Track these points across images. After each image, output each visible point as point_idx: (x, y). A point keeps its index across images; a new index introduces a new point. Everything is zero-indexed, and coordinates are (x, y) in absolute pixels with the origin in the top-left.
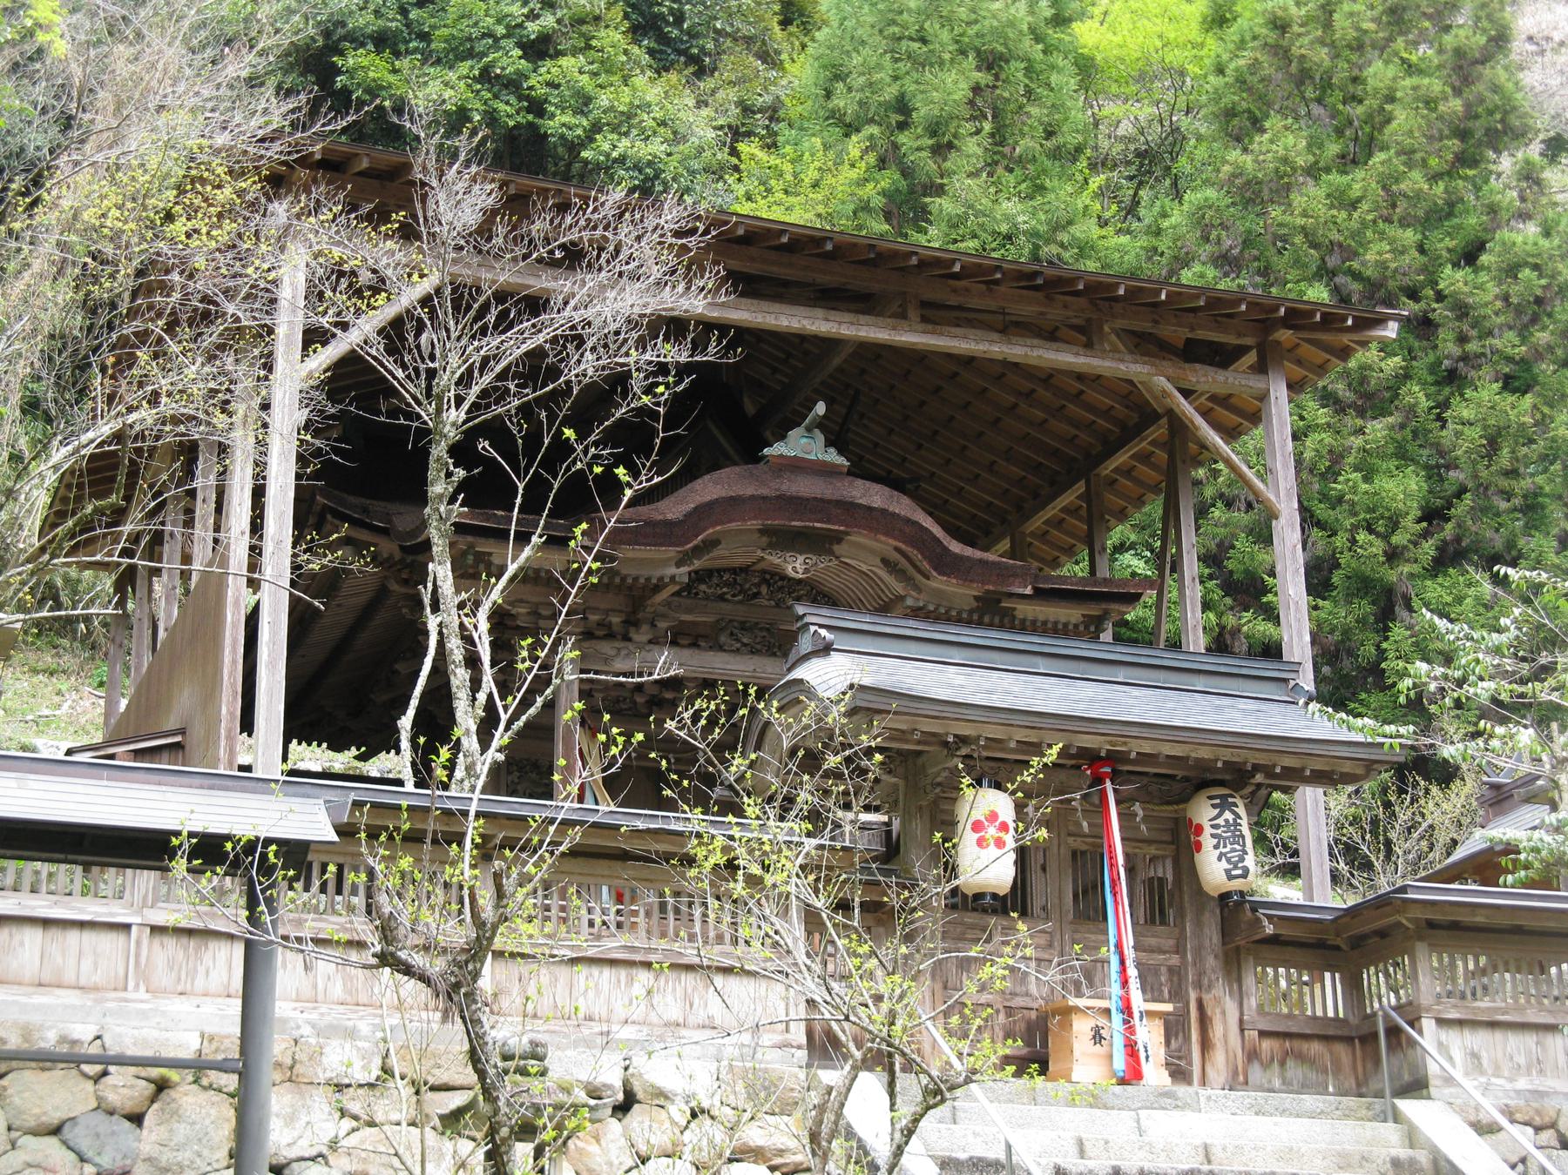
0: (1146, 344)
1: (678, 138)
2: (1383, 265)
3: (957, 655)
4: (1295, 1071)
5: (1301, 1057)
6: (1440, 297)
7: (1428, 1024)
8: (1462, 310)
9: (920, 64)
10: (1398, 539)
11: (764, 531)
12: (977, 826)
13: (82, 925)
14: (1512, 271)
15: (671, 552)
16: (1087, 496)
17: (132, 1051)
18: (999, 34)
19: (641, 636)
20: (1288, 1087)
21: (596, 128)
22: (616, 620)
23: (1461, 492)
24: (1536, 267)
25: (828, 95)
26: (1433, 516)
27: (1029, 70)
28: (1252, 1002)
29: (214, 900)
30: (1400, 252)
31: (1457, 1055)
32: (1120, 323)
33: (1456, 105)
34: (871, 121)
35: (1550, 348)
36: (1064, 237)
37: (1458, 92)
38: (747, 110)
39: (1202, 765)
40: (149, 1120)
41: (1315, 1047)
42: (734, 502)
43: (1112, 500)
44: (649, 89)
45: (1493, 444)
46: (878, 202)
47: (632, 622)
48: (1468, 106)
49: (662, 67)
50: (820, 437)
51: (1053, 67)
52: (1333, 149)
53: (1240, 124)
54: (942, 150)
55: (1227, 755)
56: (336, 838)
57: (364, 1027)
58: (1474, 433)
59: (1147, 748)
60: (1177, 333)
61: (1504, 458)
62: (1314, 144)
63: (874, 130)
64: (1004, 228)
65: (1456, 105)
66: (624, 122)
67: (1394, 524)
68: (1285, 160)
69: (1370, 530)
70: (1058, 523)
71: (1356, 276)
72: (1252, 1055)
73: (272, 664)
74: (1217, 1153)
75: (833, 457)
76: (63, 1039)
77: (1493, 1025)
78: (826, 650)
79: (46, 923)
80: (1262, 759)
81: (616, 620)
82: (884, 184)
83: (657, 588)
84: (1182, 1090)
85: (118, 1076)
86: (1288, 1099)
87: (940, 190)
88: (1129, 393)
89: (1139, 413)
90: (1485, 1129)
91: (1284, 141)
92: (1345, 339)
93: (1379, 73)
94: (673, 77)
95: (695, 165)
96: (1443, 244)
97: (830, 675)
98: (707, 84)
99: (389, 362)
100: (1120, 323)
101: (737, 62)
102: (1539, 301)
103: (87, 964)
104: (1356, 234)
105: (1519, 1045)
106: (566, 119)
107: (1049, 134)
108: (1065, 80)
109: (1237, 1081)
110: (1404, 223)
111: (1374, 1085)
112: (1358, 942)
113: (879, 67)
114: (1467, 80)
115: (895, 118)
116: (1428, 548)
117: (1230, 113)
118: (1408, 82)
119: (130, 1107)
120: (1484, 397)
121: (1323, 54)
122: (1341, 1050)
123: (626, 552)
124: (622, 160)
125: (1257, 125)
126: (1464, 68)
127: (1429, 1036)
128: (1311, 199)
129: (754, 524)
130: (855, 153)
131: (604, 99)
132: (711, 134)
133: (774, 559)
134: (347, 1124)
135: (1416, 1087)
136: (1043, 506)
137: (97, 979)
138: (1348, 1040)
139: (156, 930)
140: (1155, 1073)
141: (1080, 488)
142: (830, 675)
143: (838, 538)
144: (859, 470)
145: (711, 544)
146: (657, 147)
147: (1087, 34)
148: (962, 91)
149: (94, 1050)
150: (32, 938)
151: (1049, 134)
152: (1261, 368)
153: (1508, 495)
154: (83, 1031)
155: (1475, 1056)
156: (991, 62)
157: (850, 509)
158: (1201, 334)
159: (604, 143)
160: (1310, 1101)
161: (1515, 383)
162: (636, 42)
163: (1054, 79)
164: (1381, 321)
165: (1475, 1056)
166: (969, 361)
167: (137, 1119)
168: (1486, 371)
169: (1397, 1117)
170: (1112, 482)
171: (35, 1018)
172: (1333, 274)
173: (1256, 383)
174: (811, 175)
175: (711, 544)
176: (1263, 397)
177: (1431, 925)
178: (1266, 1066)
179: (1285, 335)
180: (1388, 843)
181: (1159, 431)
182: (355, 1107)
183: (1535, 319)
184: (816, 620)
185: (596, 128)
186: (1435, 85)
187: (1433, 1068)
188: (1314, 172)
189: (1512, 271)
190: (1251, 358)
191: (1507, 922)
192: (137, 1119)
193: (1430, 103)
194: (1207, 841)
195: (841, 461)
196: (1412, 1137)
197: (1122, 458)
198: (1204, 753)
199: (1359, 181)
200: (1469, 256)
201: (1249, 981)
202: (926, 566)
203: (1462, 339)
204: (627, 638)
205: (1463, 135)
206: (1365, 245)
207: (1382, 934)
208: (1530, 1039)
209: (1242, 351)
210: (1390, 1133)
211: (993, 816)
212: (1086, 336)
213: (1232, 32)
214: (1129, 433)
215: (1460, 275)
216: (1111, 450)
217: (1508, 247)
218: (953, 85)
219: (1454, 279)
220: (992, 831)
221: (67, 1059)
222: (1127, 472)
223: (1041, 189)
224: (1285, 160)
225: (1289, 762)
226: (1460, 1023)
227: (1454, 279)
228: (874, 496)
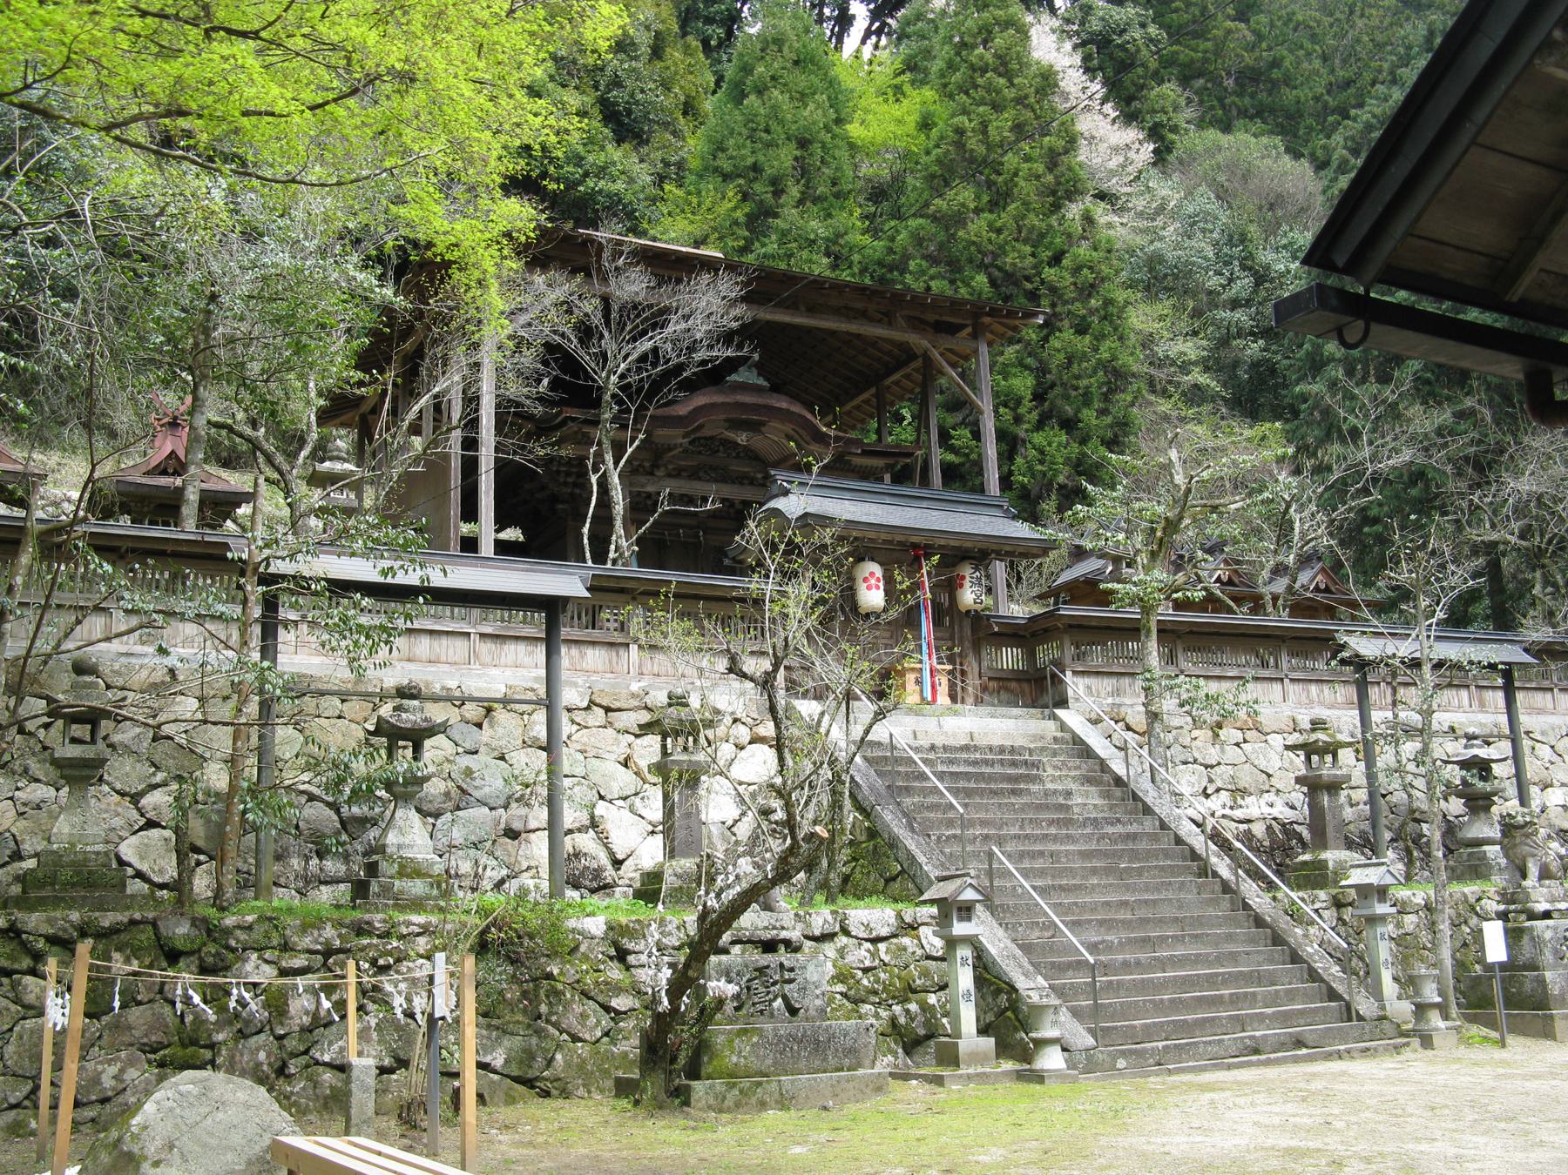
0: (917, 324)
1: (631, 181)
2: (1014, 265)
3: (848, 495)
4: (1004, 696)
5: (1007, 689)
6: (1043, 282)
7: (1069, 673)
8: (1053, 290)
9: (769, 145)
10: (1021, 410)
11: (727, 420)
12: (865, 580)
13: (447, 633)
14: (1077, 270)
15: (681, 431)
16: (877, 395)
17: (476, 694)
18: (806, 129)
19: (661, 473)
20: (1001, 703)
21: (586, 174)
22: (647, 464)
23: (1053, 386)
24: (1090, 268)
25: (715, 158)
26: (1038, 397)
27: (824, 147)
28: (985, 664)
29: (536, 624)
30: (1023, 257)
31: (1081, 687)
32: (905, 312)
33: (1050, 178)
34: (740, 176)
35: (1097, 310)
36: (842, 241)
37: (1050, 170)
38: (667, 164)
39: (967, 550)
40: (485, 725)
41: (1013, 685)
42: (713, 405)
43: (889, 397)
44: (615, 153)
45: (1070, 360)
46: (742, 219)
47: (655, 466)
48: (1056, 177)
49: (619, 141)
50: (755, 371)
51: (836, 147)
52: (985, 198)
53: (940, 181)
54: (778, 193)
55: (979, 545)
56: (588, 595)
57: (580, 681)
58: (1062, 356)
59: (942, 542)
60: (931, 317)
61: (1075, 369)
62: (978, 197)
63: (741, 181)
64: (812, 236)
65: (1050, 178)
66: (601, 172)
67: (1019, 401)
68: (963, 205)
69: (1006, 406)
70: (858, 408)
71: (1000, 269)
72: (984, 689)
73: (487, 493)
74: (976, 735)
75: (761, 382)
76: (443, 688)
77: (1098, 673)
78: (786, 493)
79: (431, 632)
80: (995, 547)
81: (647, 464)
82: (747, 210)
83: (670, 449)
84: (959, 706)
85: (468, 706)
86: (1005, 710)
87: (776, 216)
88: (905, 348)
89: (906, 355)
90: (1095, 722)
91: (964, 195)
92: (1017, 322)
93: (1011, 160)
94: (626, 146)
95: (642, 196)
96: (1046, 255)
97: (793, 505)
98: (644, 150)
99: (582, 352)
100: (905, 312)
101: (662, 137)
102: (1092, 286)
103: (451, 652)
104: (1001, 247)
105: (1107, 684)
106: (571, 169)
107: (834, 184)
108: (843, 154)
109: (978, 701)
110: (1026, 241)
111: (1041, 702)
112: (1033, 635)
113: (744, 146)
114: (1056, 165)
115: (752, 175)
116: (1034, 416)
117: (933, 176)
118: (1025, 165)
119: (475, 720)
120: (1065, 338)
121: (982, 150)
122: (1026, 686)
123: (660, 432)
124: (601, 191)
125: (947, 184)
126: (1053, 160)
127: (1069, 678)
128: (977, 227)
129: (723, 417)
130: (731, 194)
131: (591, 158)
132: (649, 179)
133: (730, 435)
134: (575, 727)
135: (1063, 703)
136: (852, 399)
137: (456, 658)
138: (1029, 681)
139: (482, 635)
140: (943, 699)
141: (873, 390)
142: (793, 505)
143: (763, 424)
144: (775, 389)
145: (701, 427)
146: (620, 186)
147: (854, 130)
148: (789, 163)
149: (457, 694)
150: (425, 641)
151: (834, 184)
152: (975, 336)
153: (1076, 389)
154: (452, 684)
155: (1089, 688)
156: (803, 143)
157: (771, 410)
158: (945, 318)
159: (590, 183)
160: (1016, 711)
161: (1081, 330)
162: (606, 126)
163: (837, 153)
164: (1035, 315)
165: (1089, 688)
166: (833, 333)
167: (479, 726)
168: (1066, 323)
169: (1055, 717)
170: (889, 388)
171: (430, 678)
172: (987, 267)
173: (972, 344)
174: (708, 202)
175: (701, 427)
176: (976, 351)
177: (1071, 626)
178: (991, 694)
179: (987, 320)
180: (1019, 573)
181: (918, 363)
182: (578, 720)
183: (1090, 296)
184: (781, 477)
185: (586, 174)
186: (1040, 168)
187: (1070, 693)
188: (977, 211)
189: (1077, 270)
190: (969, 330)
191: (1104, 624)
192: (479, 726)
193: (1038, 177)
194: (967, 584)
195: (765, 383)
196: (1063, 727)
197: (896, 377)
198: (969, 545)
199: (1005, 218)
200: (1056, 260)
201: (984, 653)
202: (808, 438)
203: (1053, 305)
204: (652, 474)
205: (1054, 193)
206: (1005, 253)
207: (1046, 630)
208: (1114, 680)
209: (961, 327)
210: (1051, 724)
211: (872, 574)
212: (887, 318)
213: (935, 132)
214: (900, 365)
215: (1052, 271)
216: (889, 373)
217: (1077, 256)
218: (784, 158)
219: (1049, 273)
220: (873, 581)
221: (447, 698)
222: (897, 383)
223: (829, 216)
224: (963, 205)
225: (1008, 548)
226: (1083, 672)
227: (1049, 273)
228: (782, 403)
